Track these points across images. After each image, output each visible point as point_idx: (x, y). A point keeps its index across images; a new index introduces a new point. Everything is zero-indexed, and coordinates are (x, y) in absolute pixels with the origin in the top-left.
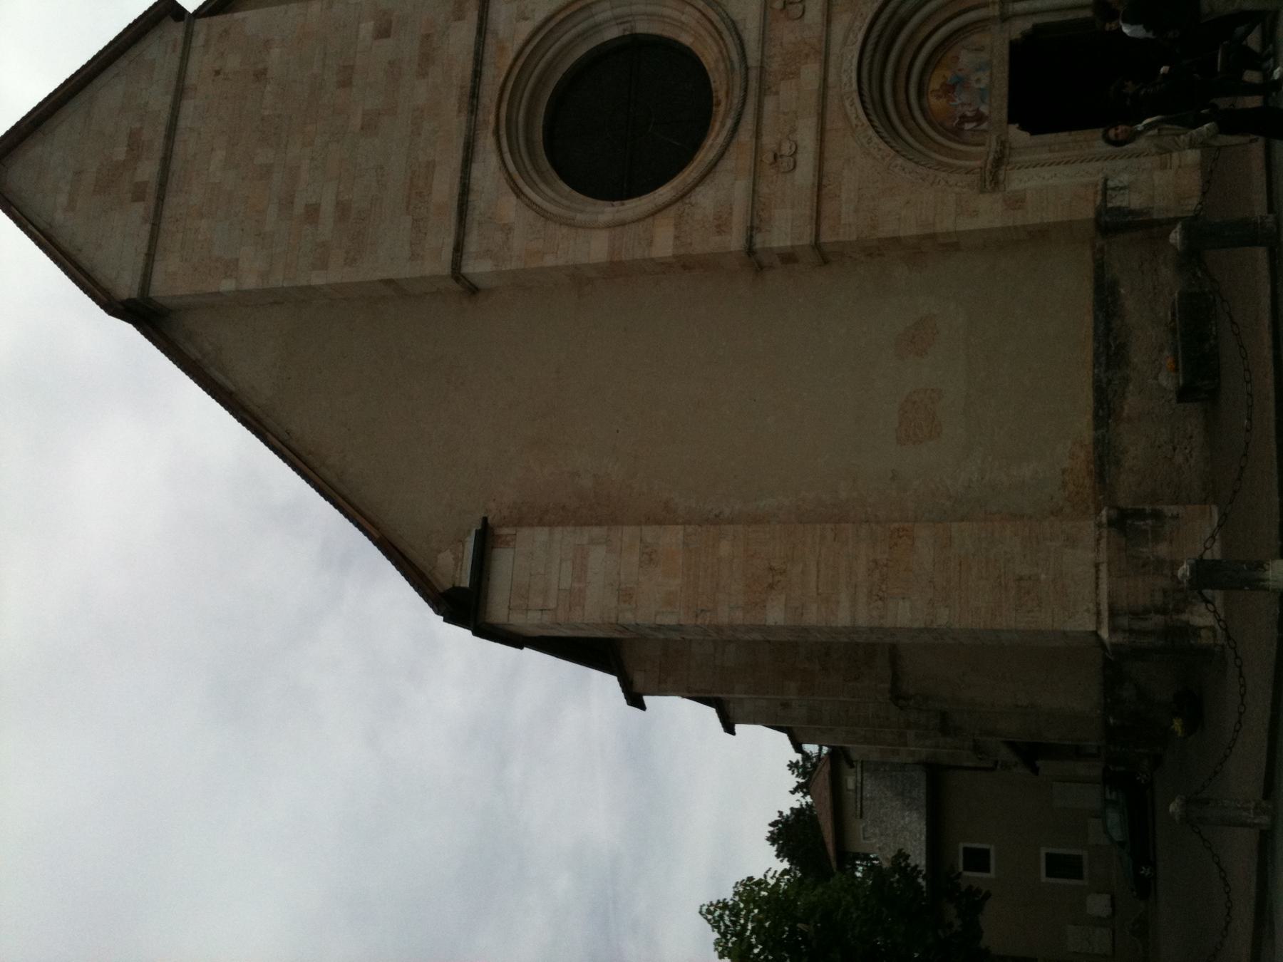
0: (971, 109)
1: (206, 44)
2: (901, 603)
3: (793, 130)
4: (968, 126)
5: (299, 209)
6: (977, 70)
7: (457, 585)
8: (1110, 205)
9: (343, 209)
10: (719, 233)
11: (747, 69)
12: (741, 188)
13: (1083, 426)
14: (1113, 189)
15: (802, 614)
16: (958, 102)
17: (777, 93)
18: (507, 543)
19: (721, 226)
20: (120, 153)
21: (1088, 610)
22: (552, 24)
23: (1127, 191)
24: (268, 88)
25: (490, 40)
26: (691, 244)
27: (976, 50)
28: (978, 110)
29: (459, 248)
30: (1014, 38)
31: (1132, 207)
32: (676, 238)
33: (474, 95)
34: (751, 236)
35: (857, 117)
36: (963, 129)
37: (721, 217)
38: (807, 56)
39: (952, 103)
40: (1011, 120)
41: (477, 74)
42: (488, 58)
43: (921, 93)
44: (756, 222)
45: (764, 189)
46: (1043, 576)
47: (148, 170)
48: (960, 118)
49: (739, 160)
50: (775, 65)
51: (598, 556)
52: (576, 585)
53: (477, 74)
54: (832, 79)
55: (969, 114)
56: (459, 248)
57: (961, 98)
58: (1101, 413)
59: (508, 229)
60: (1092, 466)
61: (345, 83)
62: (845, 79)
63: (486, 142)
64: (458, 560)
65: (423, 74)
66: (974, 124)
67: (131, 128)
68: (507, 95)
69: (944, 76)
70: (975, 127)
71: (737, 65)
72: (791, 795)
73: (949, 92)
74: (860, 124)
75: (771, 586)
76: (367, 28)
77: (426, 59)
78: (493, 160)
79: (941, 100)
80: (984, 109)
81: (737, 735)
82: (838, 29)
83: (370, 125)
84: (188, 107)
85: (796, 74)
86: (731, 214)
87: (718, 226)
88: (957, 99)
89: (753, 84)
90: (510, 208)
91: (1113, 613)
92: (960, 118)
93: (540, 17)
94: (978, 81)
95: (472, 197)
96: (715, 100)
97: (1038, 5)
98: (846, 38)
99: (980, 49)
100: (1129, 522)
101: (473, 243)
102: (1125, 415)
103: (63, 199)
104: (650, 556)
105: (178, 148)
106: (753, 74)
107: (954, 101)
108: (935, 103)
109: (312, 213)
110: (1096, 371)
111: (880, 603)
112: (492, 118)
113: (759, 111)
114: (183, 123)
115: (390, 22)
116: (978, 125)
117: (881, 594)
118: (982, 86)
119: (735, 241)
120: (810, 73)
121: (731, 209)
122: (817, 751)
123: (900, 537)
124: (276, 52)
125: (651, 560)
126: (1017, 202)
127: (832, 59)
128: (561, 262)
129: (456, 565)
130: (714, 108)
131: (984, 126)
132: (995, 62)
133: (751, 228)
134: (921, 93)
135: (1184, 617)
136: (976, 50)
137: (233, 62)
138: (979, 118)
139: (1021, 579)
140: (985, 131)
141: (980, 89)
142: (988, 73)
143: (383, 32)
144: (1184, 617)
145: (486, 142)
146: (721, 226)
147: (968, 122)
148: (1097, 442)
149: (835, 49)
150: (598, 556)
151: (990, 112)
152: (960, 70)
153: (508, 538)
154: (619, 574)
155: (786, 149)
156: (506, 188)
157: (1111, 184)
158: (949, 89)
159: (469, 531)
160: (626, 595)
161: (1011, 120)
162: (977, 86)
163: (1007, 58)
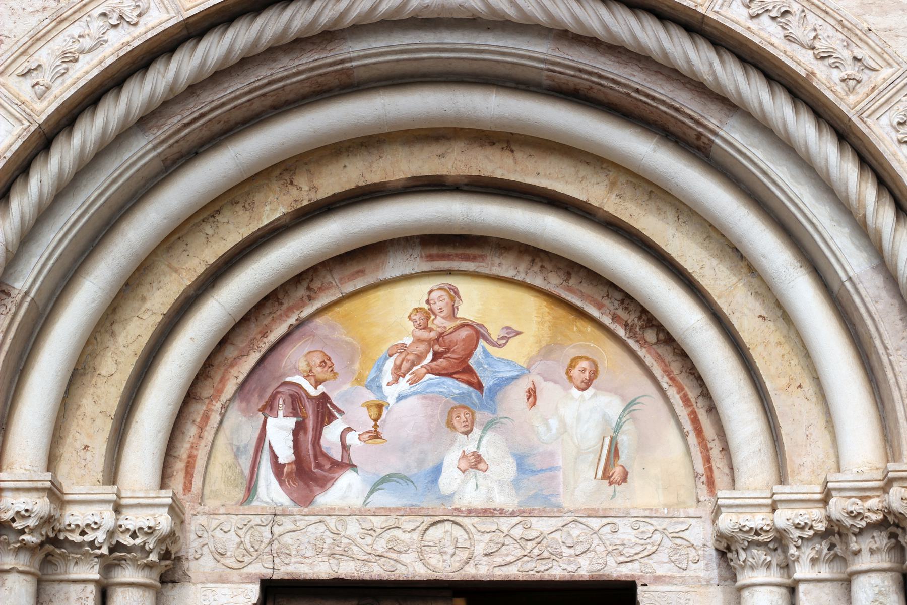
6: (523, 465)
16: (390, 393)
27: (614, 452)
28: (346, 465)
35: (69, 59)
36: (269, 408)
39: (389, 365)
48: (324, 397)
55: (331, 434)
66: (286, 455)
67: (717, 265)
69: (511, 333)
70: (274, 457)
72: (897, 143)
73: (437, 356)
88: (403, 385)
94: (476, 462)
107: (398, 373)
116: (278, 468)
118: (450, 479)
132: (541, 525)
136: (614, 452)
140: (251, 488)
141: (437, 471)
142: (503, 499)
147: (297, 431)
151: (330, 512)
152: (532, 394)
162: (452, 459)
163: (557, 571)
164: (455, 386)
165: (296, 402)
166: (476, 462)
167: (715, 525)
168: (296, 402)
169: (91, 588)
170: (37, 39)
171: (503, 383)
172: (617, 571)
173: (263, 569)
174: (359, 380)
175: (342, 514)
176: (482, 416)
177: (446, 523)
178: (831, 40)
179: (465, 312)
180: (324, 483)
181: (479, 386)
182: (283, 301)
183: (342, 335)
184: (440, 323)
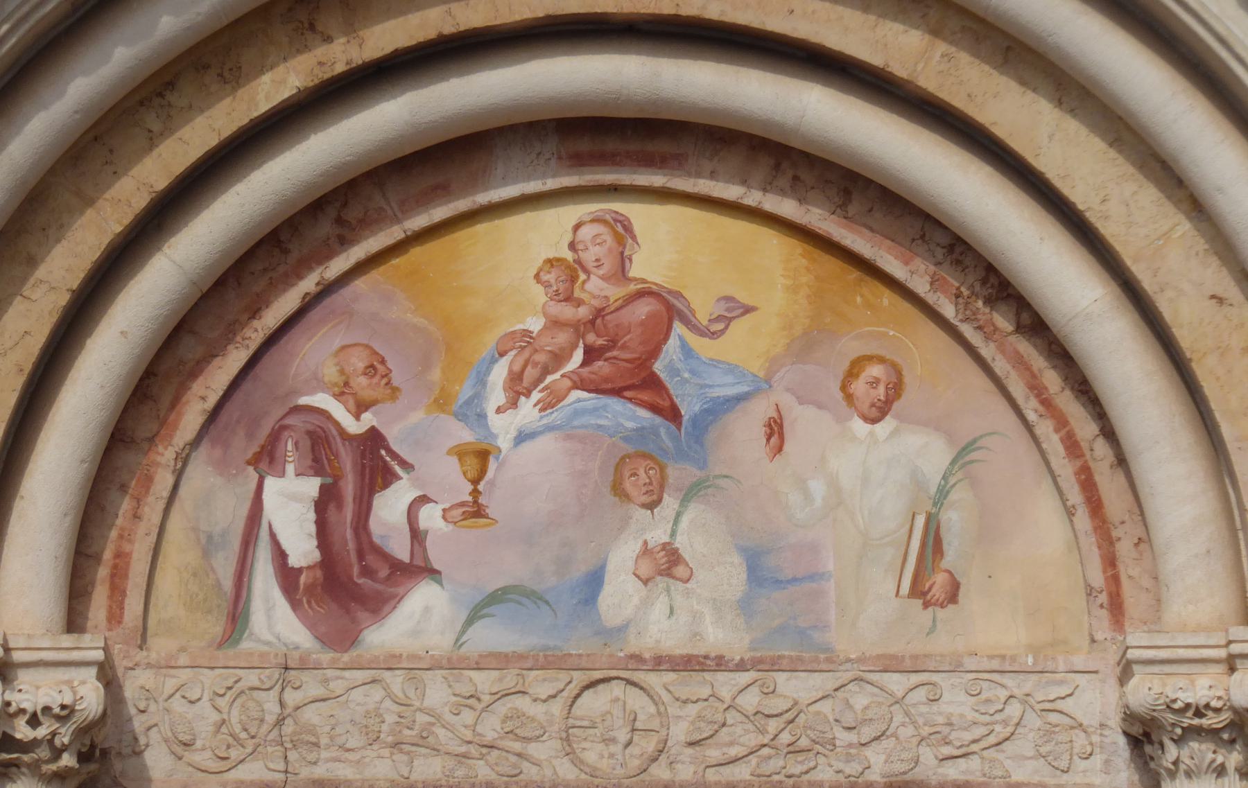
0: (430, 517)
16: (503, 427)
27: (933, 544)
39: (499, 373)
48: (374, 438)
69: (739, 309)
70: (280, 555)
73: (591, 355)
79: (539, 295)
81: (926, 611)
92: (374, 438)
97: (1244, 560)
107: (517, 388)
110: (1203, 734)
116: (287, 576)
122: (316, 556)
136: (933, 544)
141: (595, 580)
147: (325, 503)
152: (775, 430)
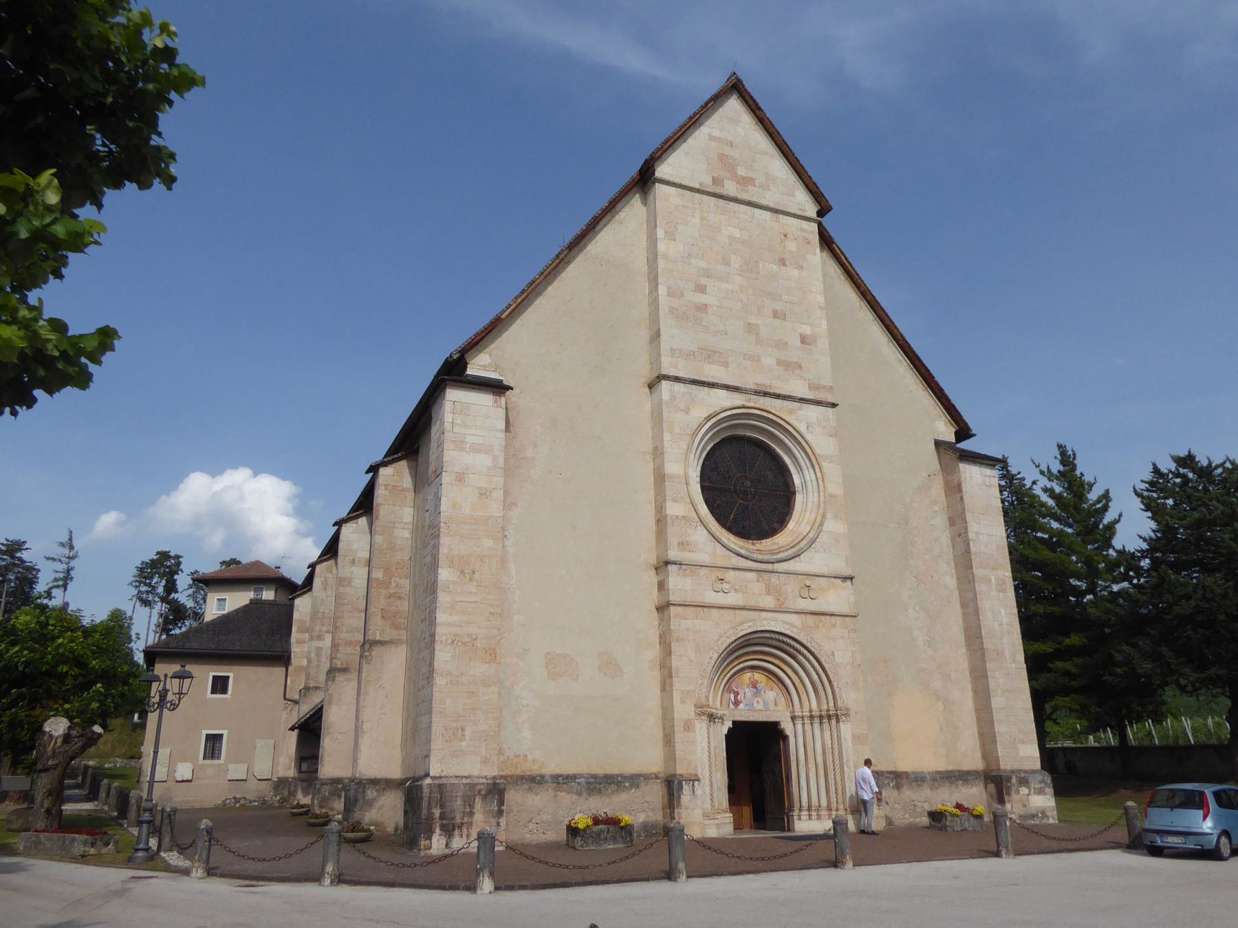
1: (802, 230)
2: (451, 654)
3: (736, 591)
4: (732, 696)
5: (703, 281)
7: (468, 366)
8: (684, 783)
9: (703, 308)
10: (679, 544)
11: (773, 563)
12: (704, 558)
13: (551, 768)
14: (693, 785)
15: (444, 591)
17: (758, 581)
18: (496, 402)
19: (683, 545)
20: (741, 172)
21: (442, 771)
22: (804, 443)
23: (692, 793)
24: (775, 267)
25: (797, 405)
26: (673, 526)
28: (741, 702)
29: (677, 379)
30: (781, 724)
31: (682, 796)
32: (677, 517)
33: (766, 394)
34: (676, 564)
36: (730, 693)
37: (688, 545)
38: (778, 600)
40: (734, 723)
41: (778, 396)
42: (786, 403)
43: (753, 668)
44: (684, 567)
45: (703, 571)
46: (464, 743)
47: (731, 189)
49: (722, 557)
50: (774, 579)
51: (485, 460)
52: (468, 446)
53: (778, 396)
54: (764, 614)
55: (739, 697)
56: (677, 379)
57: (749, 691)
58: (560, 779)
59: (687, 411)
60: (528, 773)
61: (775, 314)
62: (765, 622)
63: (737, 400)
64: (484, 367)
65: (779, 363)
66: (733, 700)
68: (764, 414)
71: (775, 557)
74: (738, 631)
75: (462, 572)
76: (807, 330)
77: (789, 366)
78: (728, 404)
80: (741, 706)
82: (793, 618)
83: (751, 328)
84: (767, 215)
85: (768, 593)
86: (689, 551)
87: (683, 544)
89: (764, 566)
90: (700, 413)
91: (440, 786)
93: (808, 437)
95: (706, 389)
96: (755, 542)
98: (788, 623)
99: (776, 705)
100: (497, 797)
101: (679, 387)
102: (559, 793)
103: (716, 133)
104: (484, 494)
105: (743, 208)
106: (769, 567)
108: (747, 676)
109: (701, 289)
111: (450, 641)
112: (752, 404)
113: (748, 570)
114: (757, 211)
115: (810, 345)
117: (456, 642)
119: (673, 554)
120: (769, 602)
121: (693, 552)
123: (490, 655)
124: (796, 272)
125: (482, 495)
126: (688, 727)
127: (775, 615)
128: (666, 444)
129: (481, 366)
130: (751, 541)
131: (731, 706)
132: (768, 712)
133: (681, 564)
134: (753, 668)
135: (438, 831)
137: (791, 246)
138: (737, 703)
139: (463, 730)
143: (804, 340)
144: (438, 831)
145: (737, 400)
146: (683, 545)
148: (542, 777)
149: (781, 616)
150: (485, 460)
151: (739, 710)
152: (765, 692)
153: (498, 403)
154: (474, 473)
155: (725, 586)
156: (711, 411)
157: (696, 783)
158: (754, 685)
159: (502, 375)
160: (460, 478)
161: (734, 723)
164: (755, 690)
165: (734, 692)
166: (758, 702)
167: (668, 739)
168: (734, 692)
169: (270, 778)
170: (718, 640)
171: (761, 690)
172: (778, 720)
173: (732, 719)
174: (742, 689)
175: (742, 710)
176: (758, 695)
177: (180, 780)
178: (816, 646)
179: (755, 678)
180: (739, 705)
181: (757, 690)
182: (38, 576)
183: (17, 603)
184: (752, 680)
